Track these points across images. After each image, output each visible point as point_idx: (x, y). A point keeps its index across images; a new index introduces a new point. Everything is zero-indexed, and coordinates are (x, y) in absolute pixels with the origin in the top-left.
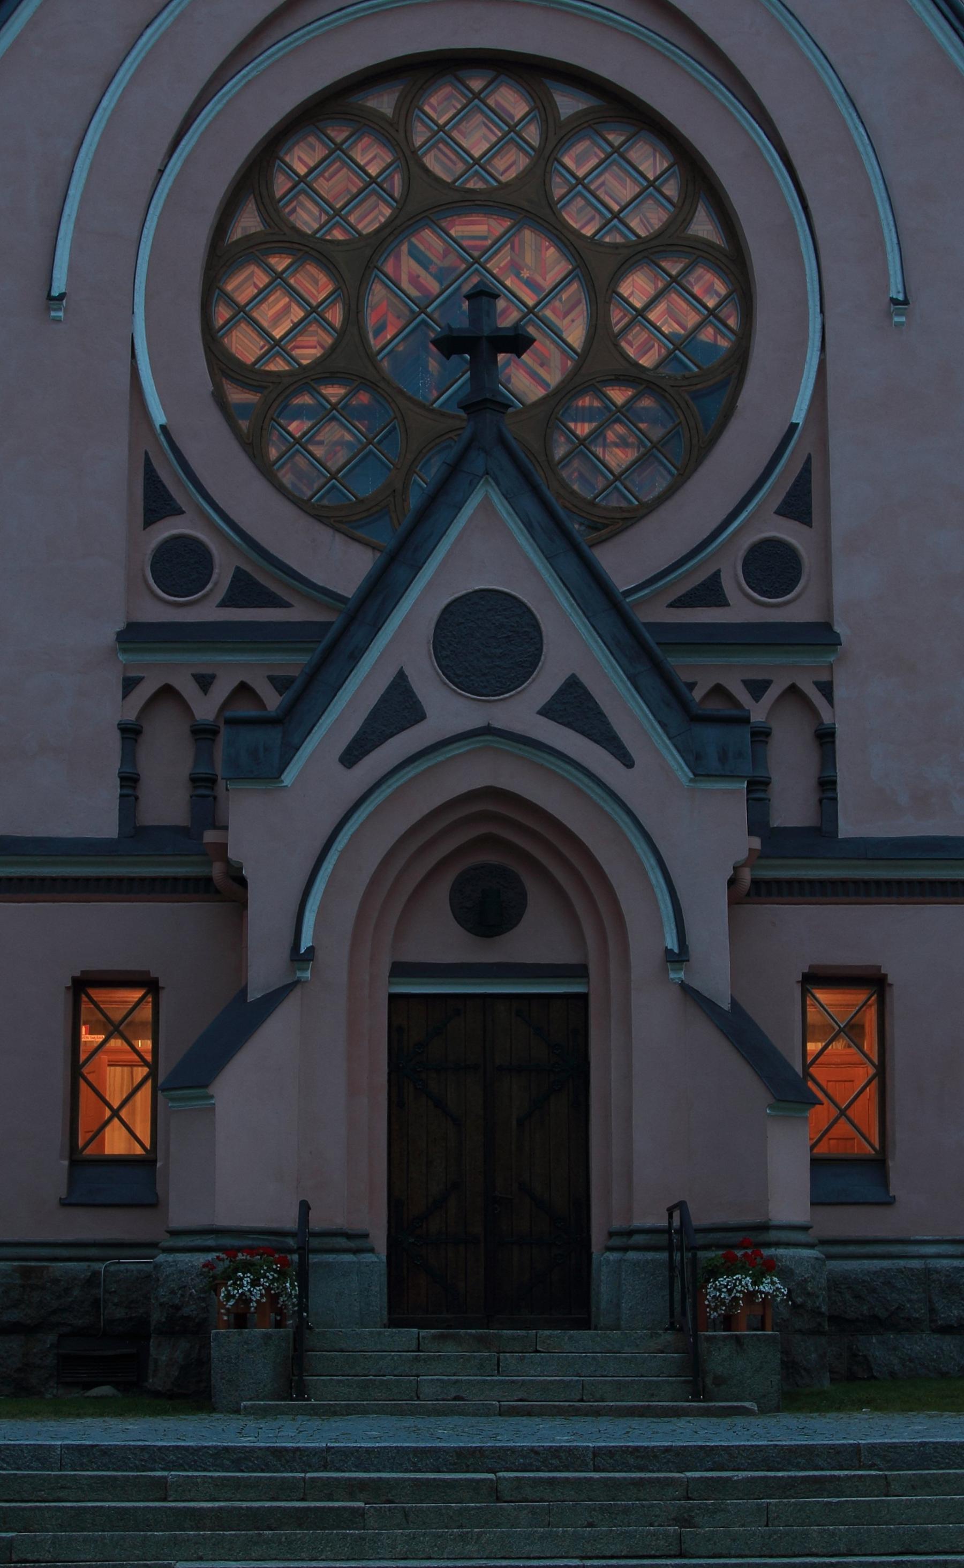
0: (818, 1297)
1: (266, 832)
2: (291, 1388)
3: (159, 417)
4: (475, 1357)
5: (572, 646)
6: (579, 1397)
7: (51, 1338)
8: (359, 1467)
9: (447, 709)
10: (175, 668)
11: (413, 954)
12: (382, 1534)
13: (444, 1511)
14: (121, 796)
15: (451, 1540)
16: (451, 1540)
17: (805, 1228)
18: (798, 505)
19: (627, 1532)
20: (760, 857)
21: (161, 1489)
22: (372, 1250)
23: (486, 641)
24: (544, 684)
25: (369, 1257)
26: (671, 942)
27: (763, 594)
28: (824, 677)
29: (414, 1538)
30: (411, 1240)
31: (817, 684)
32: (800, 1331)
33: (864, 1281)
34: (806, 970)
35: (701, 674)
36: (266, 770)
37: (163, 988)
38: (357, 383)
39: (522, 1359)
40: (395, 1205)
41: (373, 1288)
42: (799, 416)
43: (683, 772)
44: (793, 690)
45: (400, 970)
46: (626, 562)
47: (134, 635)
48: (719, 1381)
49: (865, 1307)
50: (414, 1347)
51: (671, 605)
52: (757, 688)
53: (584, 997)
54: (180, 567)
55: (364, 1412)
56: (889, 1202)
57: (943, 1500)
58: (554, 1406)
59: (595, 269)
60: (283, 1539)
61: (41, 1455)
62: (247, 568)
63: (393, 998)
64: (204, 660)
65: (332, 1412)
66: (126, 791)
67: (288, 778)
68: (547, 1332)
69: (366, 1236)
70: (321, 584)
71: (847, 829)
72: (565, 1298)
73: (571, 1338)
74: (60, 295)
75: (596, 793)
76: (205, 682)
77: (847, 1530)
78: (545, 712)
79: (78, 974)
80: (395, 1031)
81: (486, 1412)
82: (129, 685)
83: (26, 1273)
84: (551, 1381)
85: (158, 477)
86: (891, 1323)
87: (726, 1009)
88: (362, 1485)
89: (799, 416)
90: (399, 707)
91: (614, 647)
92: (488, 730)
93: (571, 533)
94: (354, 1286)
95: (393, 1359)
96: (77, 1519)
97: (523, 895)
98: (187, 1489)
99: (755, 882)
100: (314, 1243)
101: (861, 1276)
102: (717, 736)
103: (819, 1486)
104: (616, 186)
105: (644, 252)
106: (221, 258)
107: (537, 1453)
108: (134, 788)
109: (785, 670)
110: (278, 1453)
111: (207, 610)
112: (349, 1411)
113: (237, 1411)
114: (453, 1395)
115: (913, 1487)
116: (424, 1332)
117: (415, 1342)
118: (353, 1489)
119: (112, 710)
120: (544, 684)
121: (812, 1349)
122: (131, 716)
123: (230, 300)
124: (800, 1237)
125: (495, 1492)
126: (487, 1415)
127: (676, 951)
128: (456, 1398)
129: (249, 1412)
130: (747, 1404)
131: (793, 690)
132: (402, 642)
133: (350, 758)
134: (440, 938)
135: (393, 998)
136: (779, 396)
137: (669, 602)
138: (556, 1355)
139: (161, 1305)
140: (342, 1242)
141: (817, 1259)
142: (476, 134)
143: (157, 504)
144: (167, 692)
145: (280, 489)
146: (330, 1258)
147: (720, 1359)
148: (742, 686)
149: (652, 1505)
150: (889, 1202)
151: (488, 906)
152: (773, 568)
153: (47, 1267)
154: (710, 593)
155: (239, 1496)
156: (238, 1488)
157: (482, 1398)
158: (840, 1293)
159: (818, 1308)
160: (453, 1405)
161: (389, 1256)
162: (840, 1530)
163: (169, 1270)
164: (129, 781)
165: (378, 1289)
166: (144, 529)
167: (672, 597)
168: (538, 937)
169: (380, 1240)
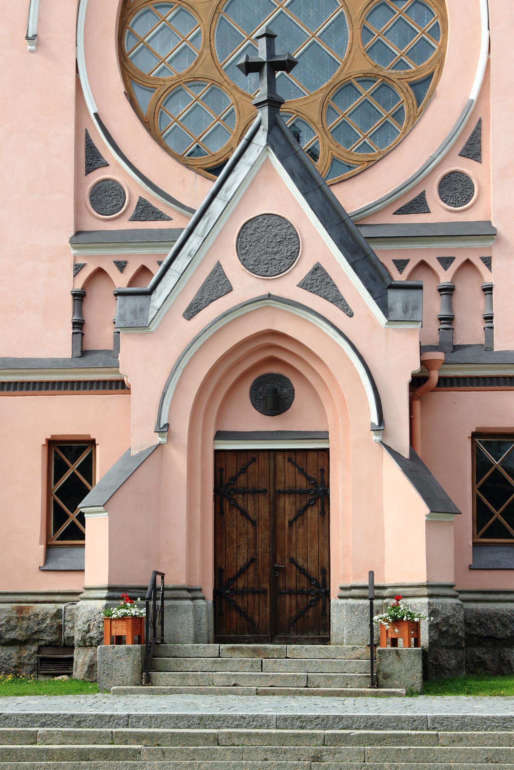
0: (457, 627)
2: (142, 679)
3: (92, 110)
4: (248, 661)
5: (319, 246)
6: (305, 685)
7: (34, 648)
8: (145, 725)
9: (245, 285)
11: (229, 427)
12: (146, 764)
13: (185, 751)
14: (73, 333)
15: (184, 767)
16: (184, 767)
17: (451, 587)
18: (473, 149)
19: (281, 764)
20: (444, 364)
21: (33, 738)
22: (203, 598)
23: (267, 245)
24: (302, 270)
25: (201, 602)
26: (375, 419)
27: (466, 202)
28: (487, 255)
29: (164, 766)
30: (228, 592)
31: (482, 259)
32: (446, 647)
33: (507, 616)
34: (474, 430)
37: (98, 444)
38: (210, 84)
39: (275, 662)
41: (202, 620)
44: (468, 262)
45: (220, 435)
48: (387, 676)
49: (509, 631)
50: (217, 655)
51: (395, 213)
52: (446, 262)
53: (326, 451)
55: (180, 692)
57: (466, 749)
58: (288, 690)
60: (93, 766)
62: (145, 197)
63: (217, 452)
66: (75, 331)
68: (294, 646)
69: (200, 590)
70: (188, 206)
71: (499, 346)
72: (314, 625)
73: (306, 650)
74: (33, 36)
76: (121, 266)
77: (405, 765)
79: (49, 437)
80: (218, 472)
81: (249, 693)
82: (78, 268)
83: (20, 610)
84: (289, 676)
85: (93, 144)
87: (407, 458)
90: (217, 285)
92: (270, 296)
94: (187, 619)
95: (202, 662)
97: (293, 391)
98: (48, 737)
99: (440, 378)
100: (167, 594)
101: (506, 612)
107: (244, 718)
108: (81, 329)
109: (461, 251)
110: (100, 717)
112: (172, 692)
113: (109, 692)
114: (233, 683)
115: (453, 741)
116: (223, 646)
117: (217, 652)
118: (139, 738)
119: (68, 284)
120: (302, 270)
121: (453, 657)
122: (79, 286)
123: (136, 37)
124: (448, 592)
125: (217, 740)
126: (249, 695)
127: (377, 424)
128: (234, 685)
129: (118, 693)
130: (398, 690)
135: (217, 452)
137: (394, 212)
139: (79, 630)
140: (185, 594)
141: (457, 604)
143: (92, 159)
144: (100, 272)
145: (166, 149)
146: (177, 602)
148: (437, 261)
149: (300, 749)
152: (457, 189)
153: (32, 607)
154: (419, 205)
155: (76, 742)
156: (77, 737)
157: (249, 684)
158: (493, 622)
159: (457, 633)
160: (233, 688)
161: (214, 601)
162: (401, 765)
163: (84, 610)
164: (79, 325)
165: (205, 620)
166: (86, 175)
167: (395, 209)
168: (301, 416)
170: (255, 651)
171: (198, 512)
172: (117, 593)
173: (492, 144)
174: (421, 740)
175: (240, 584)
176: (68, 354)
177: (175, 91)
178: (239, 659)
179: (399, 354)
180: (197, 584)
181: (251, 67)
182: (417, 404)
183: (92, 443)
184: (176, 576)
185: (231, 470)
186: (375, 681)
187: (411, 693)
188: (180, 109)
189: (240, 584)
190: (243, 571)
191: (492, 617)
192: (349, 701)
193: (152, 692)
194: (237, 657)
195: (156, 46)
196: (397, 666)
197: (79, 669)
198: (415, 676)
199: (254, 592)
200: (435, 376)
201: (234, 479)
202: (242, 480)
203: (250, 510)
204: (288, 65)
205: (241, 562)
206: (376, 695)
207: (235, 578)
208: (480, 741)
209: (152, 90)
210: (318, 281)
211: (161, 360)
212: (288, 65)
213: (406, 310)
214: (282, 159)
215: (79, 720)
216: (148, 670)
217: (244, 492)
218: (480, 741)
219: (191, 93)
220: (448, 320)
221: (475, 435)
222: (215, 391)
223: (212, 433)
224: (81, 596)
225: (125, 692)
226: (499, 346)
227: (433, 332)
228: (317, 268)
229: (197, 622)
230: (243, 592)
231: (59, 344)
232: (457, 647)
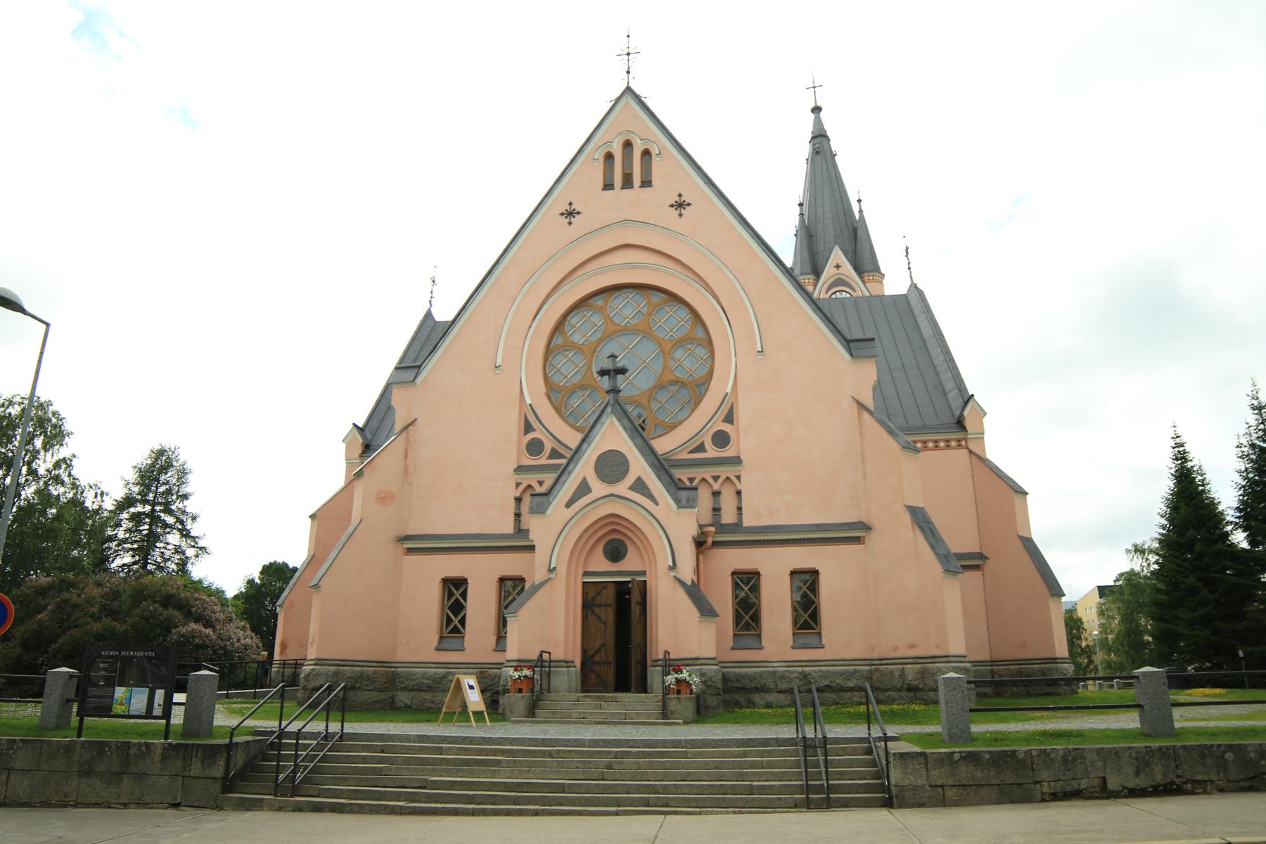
1: (541, 529)
3: (529, 402)
5: (639, 467)
9: (599, 488)
10: (531, 479)
11: (591, 569)
18: (729, 419)
21: (440, 751)
23: (612, 466)
24: (630, 479)
26: (671, 563)
35: (682, 475)
36: (539, 510)
40: (584, 651)
42: (728, 391)
43: (674, 506)
45: (586, 574)
46: (572, 438)
47: (520, 469)
48: (672, 713)
52: (716, 478)
54: (535, 447)
56: (762, 648)
59: (666, 350)
61: (408, 738)
64: (540, 476)
65: (541, 722)
67: (548, 512)
71: (746, 523)
75: (647, 515)
76: (541, 483)
78: (631, 488)
80: (585, 594)
82: (518, 485)
86: (763, 689)
88: (507, 751)
89: (728, 391)
90: (584, 489)
91: (653, 466)
92: (612, 495)
93: (638, 431)
94: (566, 679)
96: (408, 761)
98: (449, 751)
102: (682, 492)
103: (662, 755)
104: (671, 322)
105: (681, 343)
106: (549, 352)
109: (724, 472)
111: (543, 460)
118: (503, 752)
120: (630, 479)
122: (518, 495)
131: (703, 480)
132: (585, 468)
133: (568, 505)
134: (600, 563)
136: (720, 386)
138: (629, 700)
142: (626, 309)
143: (528, 428)
144: (530, 486)
147: (673, 705)
150: (762, 648)
151: (615, 552)
152: (721, 439)
154: (701, 448)
156: (466, 751)
168: (631, 563)
169: (578, 663)
170: (598, 697)
171: (571, 618)
173: (742, 415)
174: (676, 755)
175: (597, 658)
176: (511, 531)
177: (572, 392)
178: (588, 703)
179: (683, 525)
180: (570, 658)
181: (603, 373)
182: (701, 557)
184: (558, 654)
185: (592, 594)
187: (686, 723)
188: (575, 401)
189: (597, 658)
190: (598, 651)
191: (743, 676)
192: (643, 728)
193: (534, 722)
194: (588, 701)
195: (564, 370)
196: (679, 706)
199: (604, 663)
200: (710, 540)
201: (593, 599)
202: (598, 600)
203: (603, 616)
204: (622, 371)
205: (597, 646)
206: (665, 724)
207: (593, 656)
208: (712, 755)
209: (559, 392)
210: (640, 486)
211: (557, 534)
212: (622, 371)
213: (688, 501)
214: (619, 420)
216: (532, 711)
217: (599, 606)
218: (712, 755)
219: (580, 393)
220: (716, 510)
221: (733, 573)
222: (582, 548)
223: (581, 572)
224: (919, 694)
225: (518, 722)
226: (746, 523)
227: (707, 518)
228: (639, 479)
229: (569, 681)
230: (598, 663)
231: (508, 527)
232: (718, 694)
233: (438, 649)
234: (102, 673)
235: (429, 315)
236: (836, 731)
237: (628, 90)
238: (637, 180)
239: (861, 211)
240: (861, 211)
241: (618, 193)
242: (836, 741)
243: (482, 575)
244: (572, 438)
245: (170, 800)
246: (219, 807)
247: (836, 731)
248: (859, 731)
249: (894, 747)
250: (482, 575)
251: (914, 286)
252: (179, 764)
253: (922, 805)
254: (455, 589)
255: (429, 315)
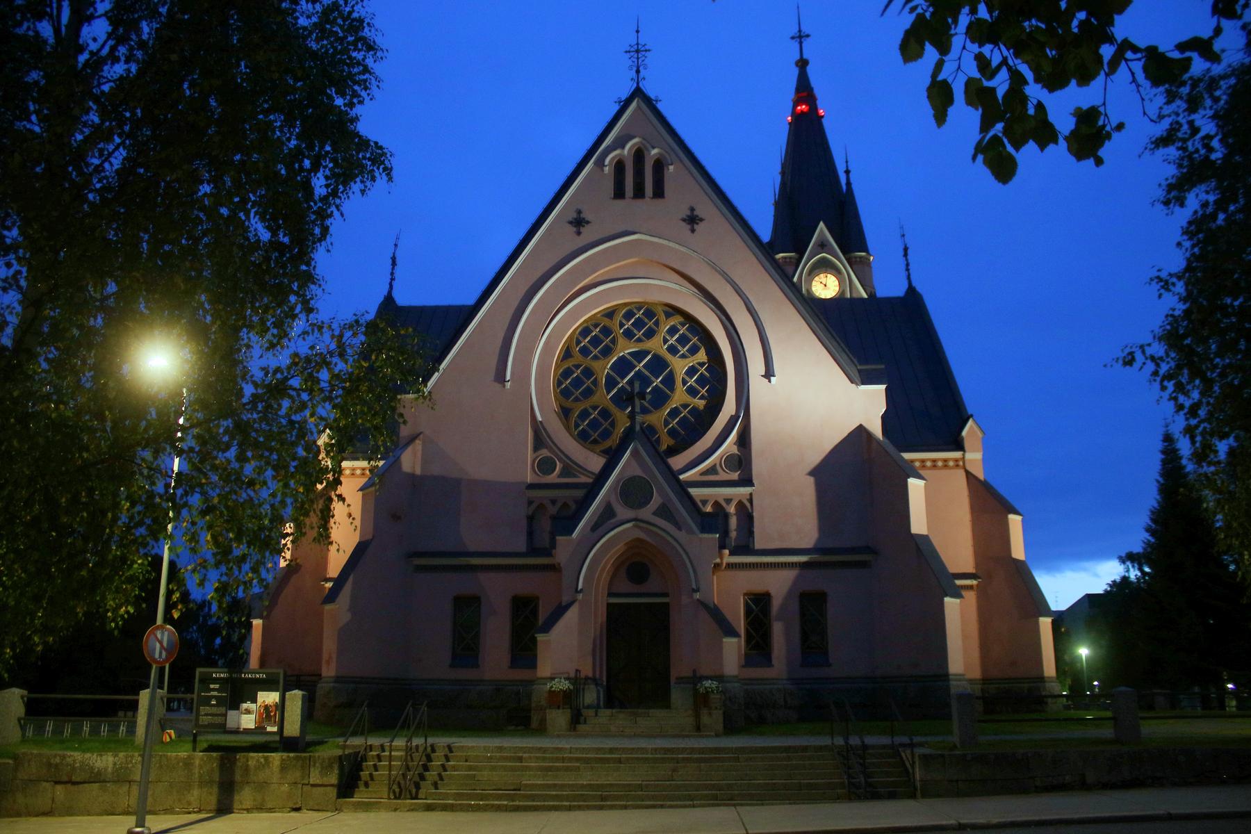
3: (540, 419)
9: (622, 512)
63: (609, 605)
78: (654, 514)
82: (530, 503)
94: (590, 696)
111: (553, 478)
118: (577, 759)
156: (544, 759)
172: (338, 679)
178: (621, 719)
183: (538, 598)
186: (698, 729)
187: (717, 735)
192: (687, 740)
197: (534, 724)
198: (720, 727)
215: (544, 750)
233: (452, 666)
234: (215, 693)
235: (389, 299)
236: (870, 740)
237: (638, 93)
238: (649, 190)
239: (847, 172)
240: (849, 184)
241: (627, 204)
242: (873, 747)
243: (498, 592)
244: (595, 463)
245: (292, 806)
246: (338, 810)
247: (870, 740)
248: (885, 740)
249: (919, 751)
250: (498, 592)
251: (911, 290)
252: (298, 774)
253: (939, 796)
254: (467, 608)
255: (389, 299)
